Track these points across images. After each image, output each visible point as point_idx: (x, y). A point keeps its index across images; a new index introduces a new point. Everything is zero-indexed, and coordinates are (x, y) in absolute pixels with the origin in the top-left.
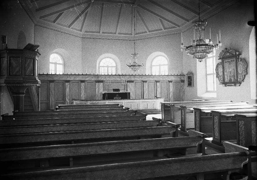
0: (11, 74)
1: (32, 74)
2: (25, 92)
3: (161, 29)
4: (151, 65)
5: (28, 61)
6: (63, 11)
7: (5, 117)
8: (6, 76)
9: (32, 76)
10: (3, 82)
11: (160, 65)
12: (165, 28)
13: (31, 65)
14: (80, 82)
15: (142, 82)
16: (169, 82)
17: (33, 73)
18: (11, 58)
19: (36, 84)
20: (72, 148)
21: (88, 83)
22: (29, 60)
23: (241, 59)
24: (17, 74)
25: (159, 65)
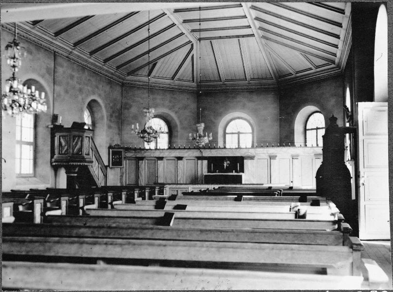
4: (305, 130)
11: (239, 133)
13: (79, 143)
18: (61, 137)
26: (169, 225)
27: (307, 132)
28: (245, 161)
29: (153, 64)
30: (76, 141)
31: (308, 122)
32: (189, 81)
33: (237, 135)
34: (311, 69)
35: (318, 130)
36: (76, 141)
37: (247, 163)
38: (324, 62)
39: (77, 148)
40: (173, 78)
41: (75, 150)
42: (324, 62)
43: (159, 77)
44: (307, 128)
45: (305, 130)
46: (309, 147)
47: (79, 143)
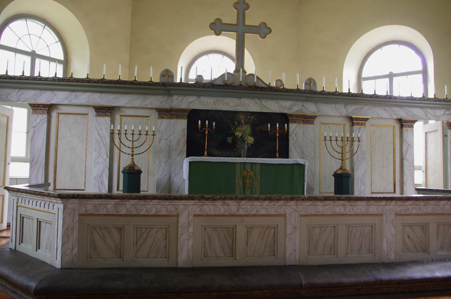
14: (92, 112)
25: (388, 73)
33: (387, 80)
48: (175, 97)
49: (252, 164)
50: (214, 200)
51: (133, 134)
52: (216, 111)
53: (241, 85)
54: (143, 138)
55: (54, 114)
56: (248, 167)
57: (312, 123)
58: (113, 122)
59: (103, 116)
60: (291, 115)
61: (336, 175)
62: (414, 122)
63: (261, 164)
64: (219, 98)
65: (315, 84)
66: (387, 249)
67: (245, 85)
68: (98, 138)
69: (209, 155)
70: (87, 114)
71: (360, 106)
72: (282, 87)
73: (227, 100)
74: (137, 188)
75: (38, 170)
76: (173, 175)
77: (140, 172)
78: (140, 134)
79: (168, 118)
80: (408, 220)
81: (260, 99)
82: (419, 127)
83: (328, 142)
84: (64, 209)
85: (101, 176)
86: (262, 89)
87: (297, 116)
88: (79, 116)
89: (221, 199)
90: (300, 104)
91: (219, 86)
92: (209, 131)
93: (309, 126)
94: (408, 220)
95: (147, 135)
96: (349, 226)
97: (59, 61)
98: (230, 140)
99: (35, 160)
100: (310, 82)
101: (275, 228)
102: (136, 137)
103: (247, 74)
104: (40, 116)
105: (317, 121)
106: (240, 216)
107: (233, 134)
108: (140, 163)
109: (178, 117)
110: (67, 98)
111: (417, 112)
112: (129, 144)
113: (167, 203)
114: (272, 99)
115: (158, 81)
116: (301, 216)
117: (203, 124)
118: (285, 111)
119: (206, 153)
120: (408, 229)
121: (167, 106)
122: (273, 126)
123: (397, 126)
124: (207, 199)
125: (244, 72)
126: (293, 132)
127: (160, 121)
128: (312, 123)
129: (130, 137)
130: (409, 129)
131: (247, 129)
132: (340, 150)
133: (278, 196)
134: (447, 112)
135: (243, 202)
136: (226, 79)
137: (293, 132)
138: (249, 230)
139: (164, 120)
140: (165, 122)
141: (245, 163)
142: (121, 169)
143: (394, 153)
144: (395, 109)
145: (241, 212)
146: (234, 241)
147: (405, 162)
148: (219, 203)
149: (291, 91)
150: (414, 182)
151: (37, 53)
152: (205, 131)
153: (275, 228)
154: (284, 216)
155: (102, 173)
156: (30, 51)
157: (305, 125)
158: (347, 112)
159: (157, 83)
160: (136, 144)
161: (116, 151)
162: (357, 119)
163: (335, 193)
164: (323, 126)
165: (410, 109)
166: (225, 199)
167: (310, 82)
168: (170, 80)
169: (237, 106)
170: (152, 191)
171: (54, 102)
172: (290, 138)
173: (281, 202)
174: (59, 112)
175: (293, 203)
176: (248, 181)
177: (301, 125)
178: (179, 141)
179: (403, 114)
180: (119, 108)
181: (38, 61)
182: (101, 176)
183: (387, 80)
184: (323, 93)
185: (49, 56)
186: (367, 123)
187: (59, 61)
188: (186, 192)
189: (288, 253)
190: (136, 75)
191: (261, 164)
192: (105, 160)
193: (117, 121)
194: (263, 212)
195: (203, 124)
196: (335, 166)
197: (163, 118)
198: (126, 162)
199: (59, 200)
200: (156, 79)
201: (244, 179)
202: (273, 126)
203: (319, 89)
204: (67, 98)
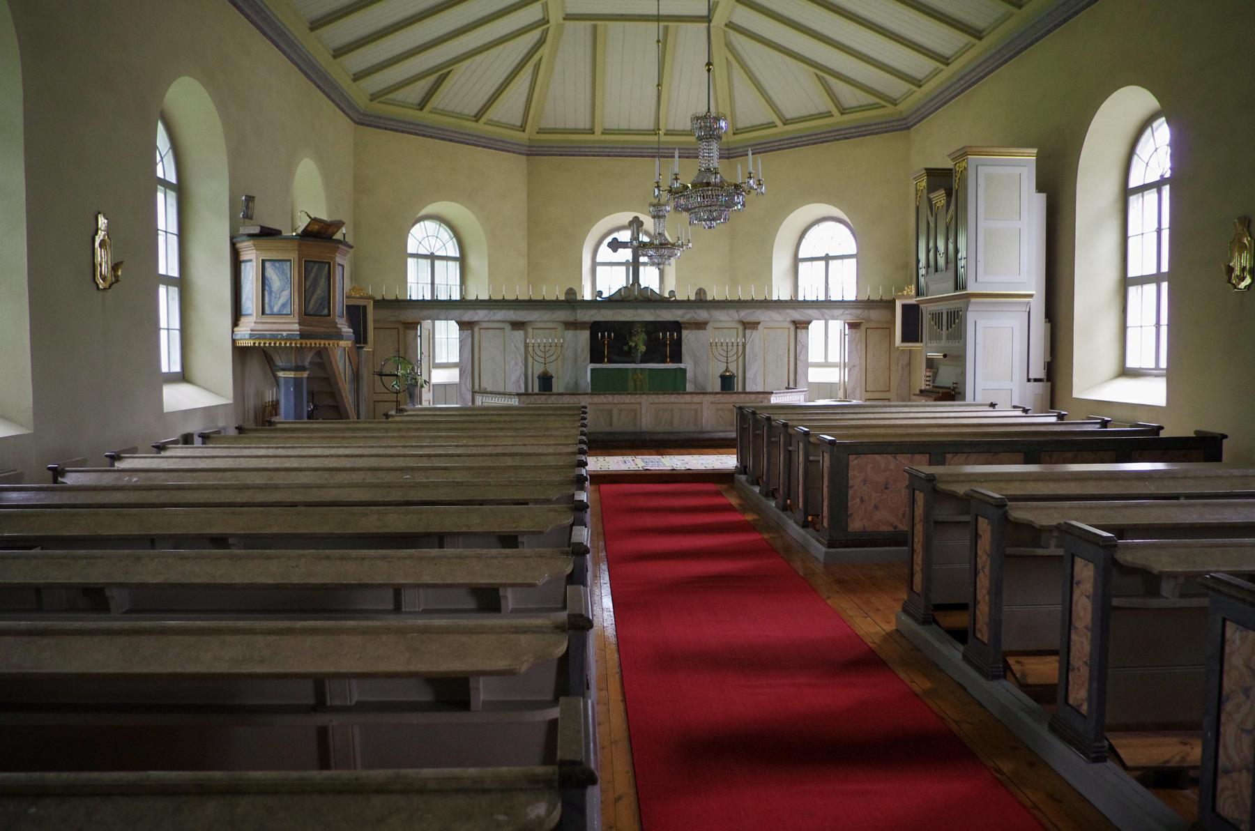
0: (267, 311)
1: (323, 308)
2: (310, 363)
3: (774, 126)
4: (796, 261)
5: (314, 270)
6: (449, 66)
7: (1245, 625)
8: (253, 319)
9: (325, 316)
10: (247, 337)
11: (827, 258)
12: (843, 111)
13: (323, 282)
14: (508, 327)
15: (741, 329)
16: (745, 328)
17: (327, 305)
18: (267, 265)
19: (338, 339)
20: (325, 472)
21: (538, 331)
22: (316, 267)
23: (356, 315)
24: (284, 312)
25: (824, 255)
26: (907, 531)
27: (599, 269)
28: (685, 333)
29: (441, 74)
30: (312, 275)
31: (804, 241)
32: (512, 127)
33: (823, 263)
34: (772, 125)
35: (832, 263)
36: (312, 275)
37: (689, 338)
38: (872, 99)
39: (315, 297)
40: (477, 117)
41: (312, 304)
42: (872, 99)
43: (444, 113)
44: (801, 256)
45: (796, 261)
46: (267, 314)
47: (323, 282)
48: (578, 311)
49: (641, 369)
50: (599, 394)
51: (545, 346)
52: (615, 322)
53: (636, 299)
54: (553, 348)
55: (476, 329)
56: (638, 372)
57: (705, 329)
58: (526, 337)
59: (518, 330)
60: (684, 323)
61: (723, 377)
62: (809, 323)
63: (650, 370)
64: (618, 310)
65: (705, 293)
66: (279, 314)
67: (641, 298)
68: (515, 349)
69: (610, 361)
70: (504, 329)
71: (752, 311)
72: (674, 298)
73: (624, 312)
74: (550, 389)
75: (467, 377)
76: (579, 379)
77: (552, 377)
78: (550, 346)
79: (574, 329)
80: (719, 406)
81: (654, 309)
82: (816, 327)
83: (714, 347)
84: (519, 401)
85: (518, 381)
86: (656, 301)
87: (689, 323)
88: (497, 330)
89: (602, 394)
90: (692, 311)
91: (616, 301)
92: (608, 341)
93: (701, 332)
94: (719, 406)
95: (556, 346)
96: (681, 410)
97: (454, 259)
98: (626, 348)
99: (463, 369)
100: (701, 292)
101: (635, 410)
102: (547, 349)
103: (642, 287)
104: (465, 331)
105: (709, 327)
106: (614, 404)
107: (627, 344)
108: (551, 370)
109: (582, 329)
110: (486, 316)
111: (812, 312)
112: (542, 355)
113: (574, 396)
114: (665, 308)
115: (564, 299)
116: (651, 404)
117: (603, 335)
118: (678, 319)
119: (606, 360)
120: (720, 412)
121: (571, 319)
122: (664, 334)
123: (792, 328)
124: (596, 394)
125: (639, 285)
126: (686, 337)
127: (566, 332)
128: (705, 329)
129: (542, 348)
130: (804, 331)
131: (643, 336)
132: (725, 354)
133: (623, 392)
134: (846, 312)
135: (616, 396)
136: (623, 294)
137: (686, 337)
138: (620, 411)
139: (570, 331)
140: (570, 334)
141: (635, 369)
142: (536, 375)
143: (789, 354)
144: (789, 311)
145: (615, 401)
146: (611, 418)
147: (798, 362)
148: (602, 396)
149: (683, 301)
150: (807, 380)
151: (436, 254)
152: (604, 341)
153: (635, 410)
154: (640, 403)
155: (519, 379)
156: (429, 254)
157: (697, 332)
158: (739, 316)
159: (563, 301)
160: (548, 355)
161: (530, 359)
162: (749, 323)
163: (540, 391)
164: (717, 331)
165: (805, 311)
166: (605, 394)
167: (701, 292)
168: (574, 297)
169: (634, 316)
170: (561, 390)
171: (476, 319)
172: (683, 344)
173: (638, 396)
174: (480, 327)
175: (645, 396)
176: (638, 383)
177: (694, 331)
178: (583, 349)
179: (797, 315)
180: (531, 322)
181: (437, 263)
182: (518, 381)
183: (823, 263)
184: (714, 301)
185: (445, 255)
186: (760, 326)
187: (454, 259)
188: (590, 391)
189: (643, 424)
190: (544, 293)
191: (649, 369)
192: (521, 368)
193: (530, 335)
194: (627, 401)
195: (603, 335)
196: (721, 369)
197: (569, 329)
198: (539, 369)
199: (516, 397)
200: (562, 297)
201: (635, 381)
202: (664, 334)
203: (709, 298)
204: (486, 316)
